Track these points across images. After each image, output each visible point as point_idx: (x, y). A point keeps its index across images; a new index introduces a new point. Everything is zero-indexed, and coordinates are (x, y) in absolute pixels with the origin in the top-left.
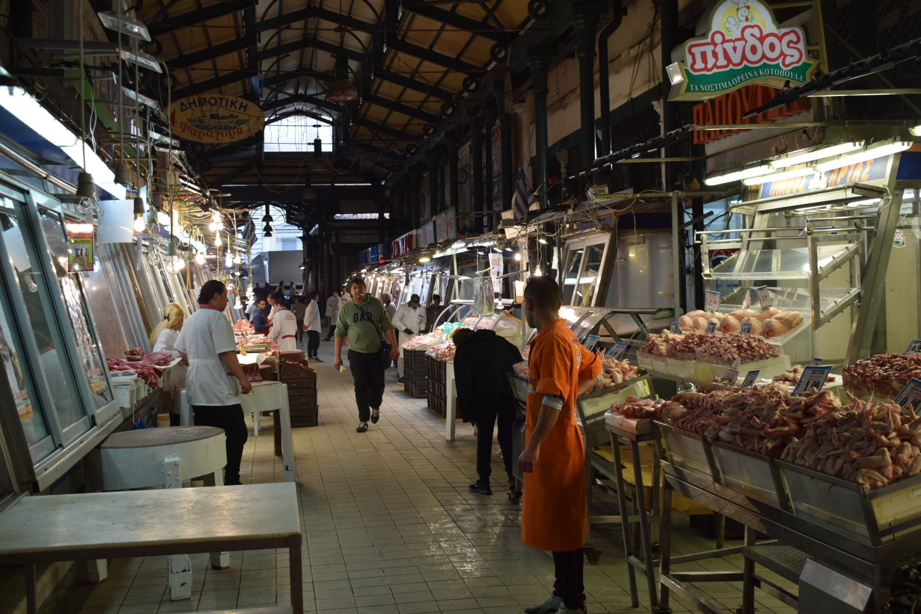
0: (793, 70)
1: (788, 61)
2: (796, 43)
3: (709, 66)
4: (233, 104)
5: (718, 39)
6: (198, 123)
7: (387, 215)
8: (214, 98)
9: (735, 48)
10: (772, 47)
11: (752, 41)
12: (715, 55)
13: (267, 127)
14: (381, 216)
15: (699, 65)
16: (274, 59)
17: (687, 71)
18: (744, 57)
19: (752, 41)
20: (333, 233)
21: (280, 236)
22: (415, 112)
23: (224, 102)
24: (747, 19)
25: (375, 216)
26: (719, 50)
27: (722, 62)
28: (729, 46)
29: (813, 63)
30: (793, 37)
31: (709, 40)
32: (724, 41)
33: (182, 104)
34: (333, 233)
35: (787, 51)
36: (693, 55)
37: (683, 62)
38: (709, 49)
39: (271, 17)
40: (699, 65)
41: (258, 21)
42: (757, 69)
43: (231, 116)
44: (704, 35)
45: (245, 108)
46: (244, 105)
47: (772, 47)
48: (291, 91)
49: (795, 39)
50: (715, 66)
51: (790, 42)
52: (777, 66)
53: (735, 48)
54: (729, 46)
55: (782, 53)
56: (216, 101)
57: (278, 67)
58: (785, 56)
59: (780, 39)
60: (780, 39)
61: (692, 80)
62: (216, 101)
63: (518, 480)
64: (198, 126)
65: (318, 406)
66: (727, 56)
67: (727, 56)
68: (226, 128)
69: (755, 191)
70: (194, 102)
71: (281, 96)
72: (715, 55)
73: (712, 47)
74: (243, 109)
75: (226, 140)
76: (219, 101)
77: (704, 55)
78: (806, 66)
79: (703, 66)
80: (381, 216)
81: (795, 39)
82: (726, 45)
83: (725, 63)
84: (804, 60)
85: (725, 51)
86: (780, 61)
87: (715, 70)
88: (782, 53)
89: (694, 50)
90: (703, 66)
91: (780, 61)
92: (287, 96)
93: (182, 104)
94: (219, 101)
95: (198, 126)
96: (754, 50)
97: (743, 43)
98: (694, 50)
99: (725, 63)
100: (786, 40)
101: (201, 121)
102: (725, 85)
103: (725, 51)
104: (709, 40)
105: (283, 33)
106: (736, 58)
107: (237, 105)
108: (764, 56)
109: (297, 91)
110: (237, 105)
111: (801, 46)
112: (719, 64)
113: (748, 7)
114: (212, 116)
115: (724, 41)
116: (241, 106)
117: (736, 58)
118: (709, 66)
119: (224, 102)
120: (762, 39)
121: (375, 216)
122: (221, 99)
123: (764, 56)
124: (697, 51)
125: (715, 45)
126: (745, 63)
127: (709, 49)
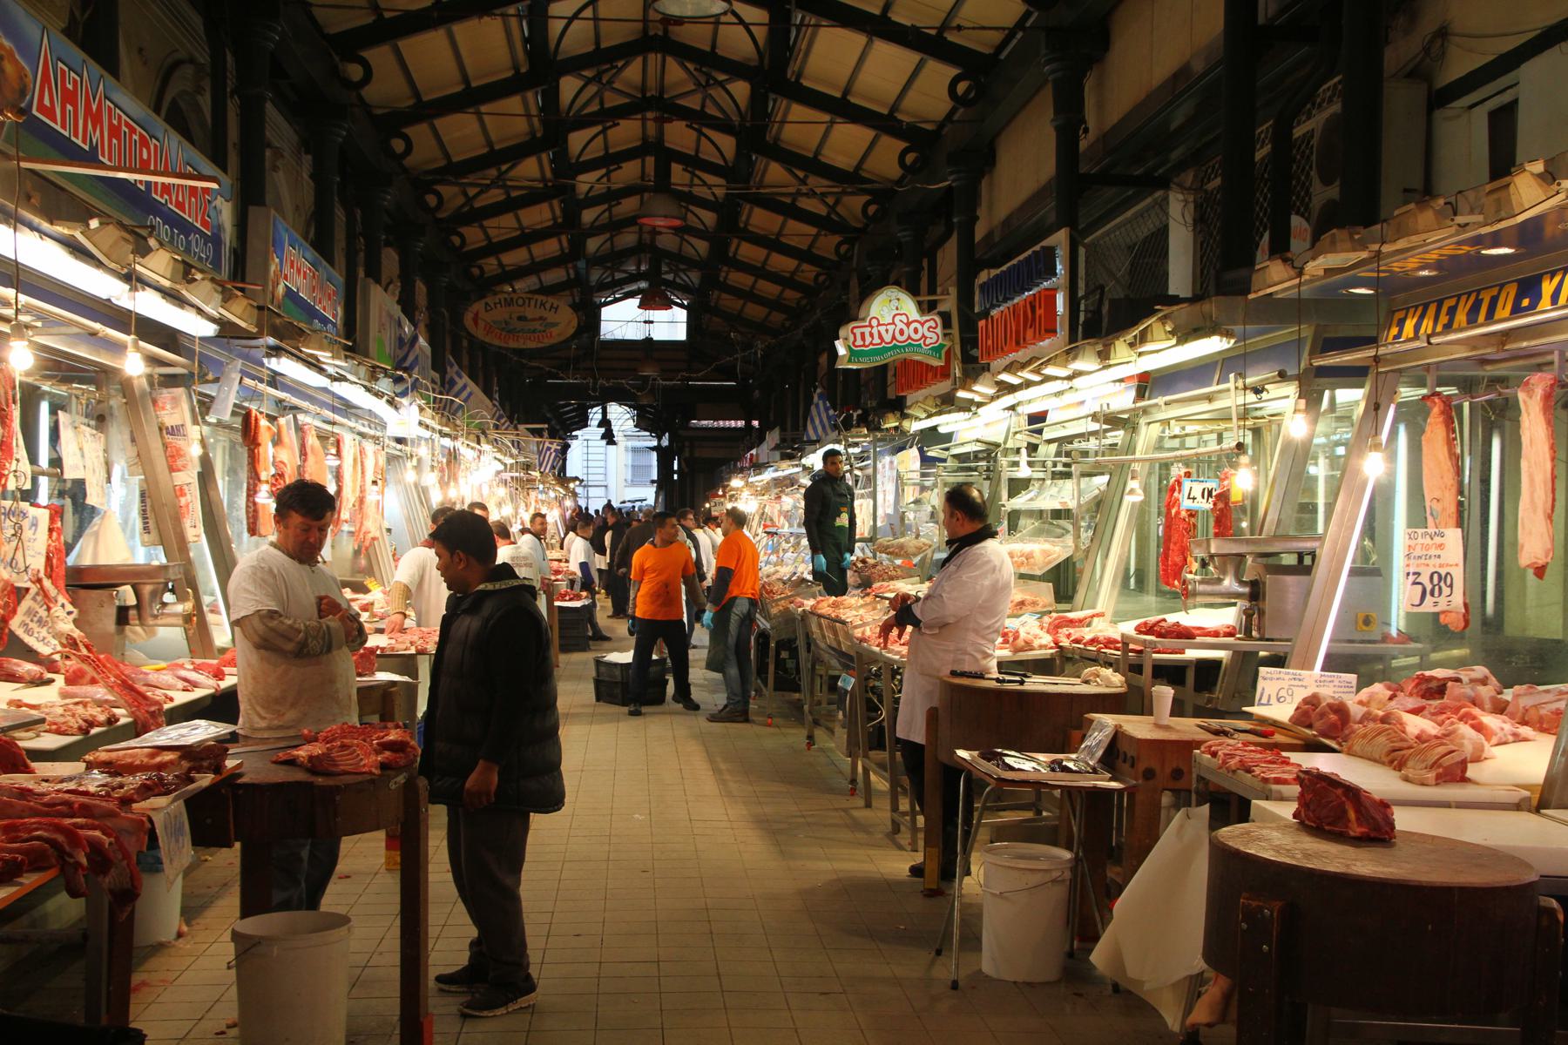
0: (932, 349)
1: (928, 342)
2: (935, 328)
3: (867, 343)
4: (543, 304)
5: (874, 323)
6: (504, 326)
7: (756, 423)
8: (518, 305)
9: (887, 331)
10: (916, 331)
11: (900, 326)
12: (871, 335)
13: (603, 309)
14: (748, 423)
15: (859, 342)
16: (607, 235)
17: (849, 346)
18: (894, 338)
19: (900, 326)
20: (687, 444)
21: (631, 444)
22: (775, 305)
23: (533, 303)
24: (897, 309)
25: (741, 424)
26: (875, 331)
27: (877, 341)
28: (882, 329)
29: (948, 344)
30: (932, 324)
31: (867, 324)
32: (879, 325)
33: (487, 304)
34: (687, 444)
35: (928, 334)
36: (854, 334)
37: (846, 339)
38: (867, 331)
39: (597, 193)
40: (859, 342)
41: (582, 197)
42: (904, 347)
43: (541, 318)
44: (864, 320)
45: (556, 309)
46: (555, 306)
47: (916, 331)
48: (632, 268)
49: (934, 325)
50: (871, 343)
51: (930, 327)
52: (919, 346)
53: (887, 331)
54: (882, 329)
55: (923, 336)
56: (524, 302)
57: (612, 244)
58: (926, 338)
59: (923, 324)
60: (923, 324)
61: (853, 354)
62: (524, 302)
63: (766, 683)
64: (503, 329)
65: (109, 300)
66: (880, 337)
67: (880, 337)
68: (534, 332)
69: (948, 437)
70: (500, 303)
71: (618, 276)
72: (871, 335)
73: (869, 329)
74: (553, 310)
75: (532, 345)
76: (527, 301)
77: (863, 334)
78: (941, 346)
79: (862, 343)
80: (748, 423)
81: (934, 325)
82: (880, 328)
83: (879, 341)
84: (940, 341)
85: (879, 332)
86: (922, 342)
87: (871, 347)
88: (923, 336)
89: (855, 331)
90: (862, 343)
91: (922, 342)
92: (624, 275)
93: (487, 304)
94: (527, 301)
95: (503, 329)
96: (902, 332)
97: (893, 326)
98: (855, 331)
99: (879, 341)
100: (927, 325)
101: (506, 323)
102: (878, 359)
103: (879, 332)
104: (867, 324)
105: (615, 239)
106: (888, 338)
107: (548, 306)
108: (909, 337)
109: (639, 268)
110: (548, 306)
111: (939, 330)
112: (874, 342)
113: (898, 299)
114: (520, 318)
115: (879, 325)
116: (552, 307)
117: (888, 338)
118: (867, 343)
119: (533, 303)
120: (908, 324)
121: (741, 424)
122: (530, 299)
123: (909, 337)
124: (858, 331)
125: (872, 327)
126: (894, 342)
127: (867, 331)
